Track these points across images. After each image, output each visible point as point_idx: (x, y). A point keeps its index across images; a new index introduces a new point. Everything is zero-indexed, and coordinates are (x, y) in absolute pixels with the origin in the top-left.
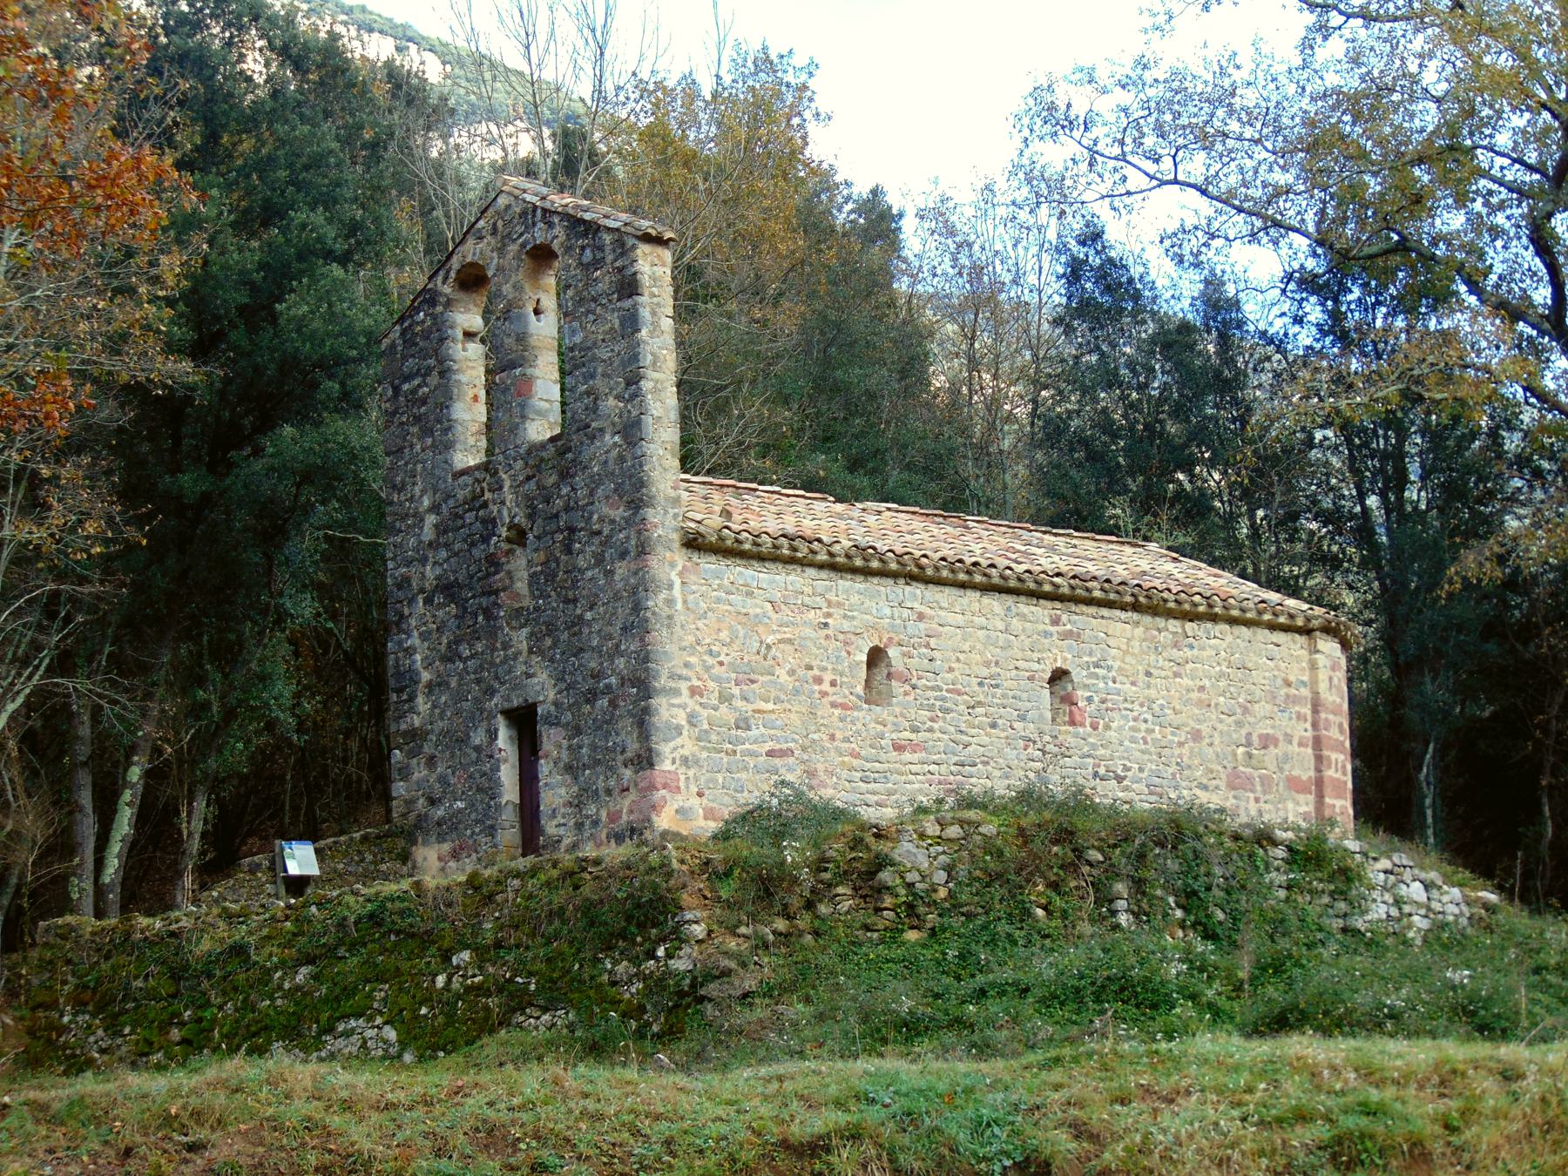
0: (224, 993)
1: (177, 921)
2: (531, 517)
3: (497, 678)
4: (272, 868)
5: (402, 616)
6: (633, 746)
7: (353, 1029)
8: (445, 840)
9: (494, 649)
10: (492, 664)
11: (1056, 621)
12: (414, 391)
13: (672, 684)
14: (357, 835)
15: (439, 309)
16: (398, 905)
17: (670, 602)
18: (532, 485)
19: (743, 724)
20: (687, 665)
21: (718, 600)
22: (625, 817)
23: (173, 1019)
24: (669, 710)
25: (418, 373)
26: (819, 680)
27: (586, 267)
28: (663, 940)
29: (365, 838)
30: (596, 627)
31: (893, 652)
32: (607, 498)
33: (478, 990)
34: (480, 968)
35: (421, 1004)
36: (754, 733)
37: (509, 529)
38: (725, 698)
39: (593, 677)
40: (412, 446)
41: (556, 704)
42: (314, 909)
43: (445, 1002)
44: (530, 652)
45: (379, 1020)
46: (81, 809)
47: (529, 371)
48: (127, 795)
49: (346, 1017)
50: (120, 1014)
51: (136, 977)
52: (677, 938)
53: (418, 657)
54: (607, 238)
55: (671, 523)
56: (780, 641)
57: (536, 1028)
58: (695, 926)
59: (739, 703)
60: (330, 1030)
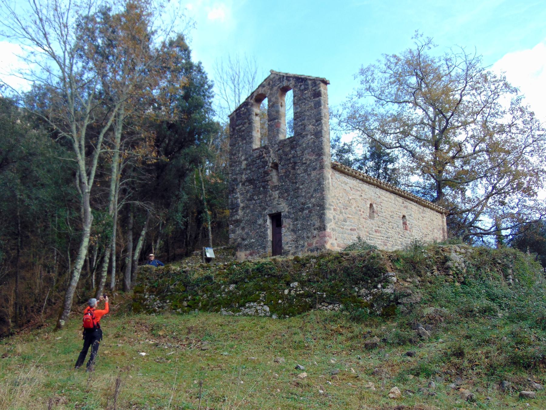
0: (203, 291)
1: (185, 268)
2: (281, 160)
3: (267, 205)
4: (202, 255)
5: (234, 189)
6: (317, 224)
7: (252, 306)
8: (247, 250)
9: (266, 197)
10: (266, 201)
11: (403, 203)
12: (240, 129)
13: (329, 207)
14: (222, 247)
15: (249, 106)
16: (269, 266)
17: (329, 183)
18: (281, 151)
19: (345, 221)
20: (333, 202)
21: (339, 185)
22: (314, 245)
23: (185, 298)
24: (329, 214)
25: (241, 124)
26: (360, 211)
27: (302, 91)
28: (380, 282)
29: (224, 248)
30: (304, 190)
31: (374, 205)
32: (309, 153)
33: (302, 295)
34: (302, 288)
35: (279, 299)
36: (347, 223)
37: (272, 163)
38: (341, 213)
39: (302, 204)
40: (238, 143)
41: (288, 212)
42: (235, 266)
43: (289, 299)
44: (279, 197)
45: (262, 304)
46: (130, 241)
47: (280, 121)
48: (141, 238)
49: (250, 302)
50: (165, 296)
51: (171, 285)
52: (386, 281)
53: (239, 200)
54: (310, 82)
55: (329, 161)
56: (353, 199)
57: (327, 310)
58: (393, 278)
59: (344, 214)
60: (243, 305)
